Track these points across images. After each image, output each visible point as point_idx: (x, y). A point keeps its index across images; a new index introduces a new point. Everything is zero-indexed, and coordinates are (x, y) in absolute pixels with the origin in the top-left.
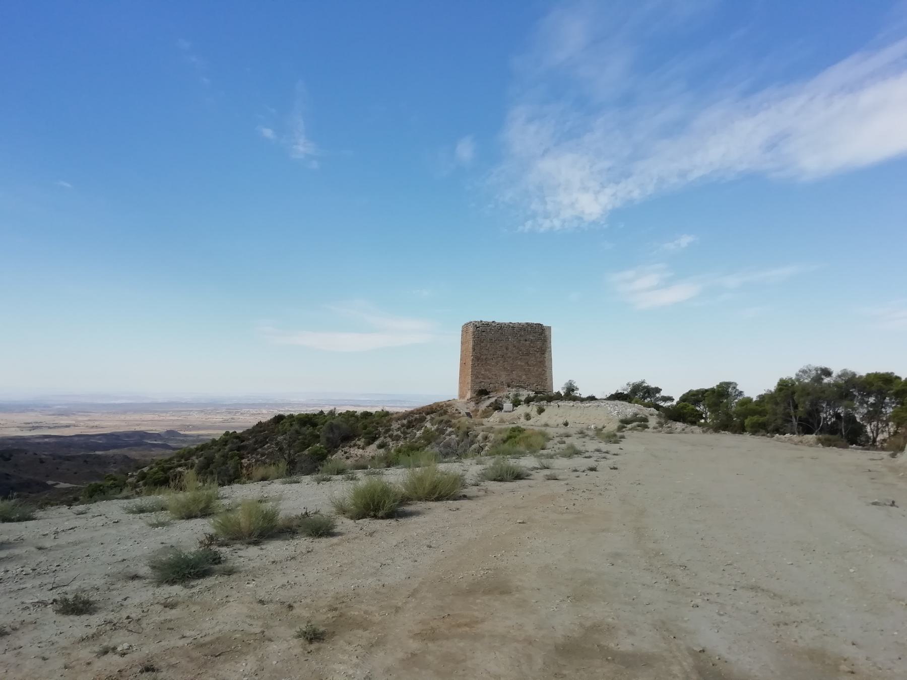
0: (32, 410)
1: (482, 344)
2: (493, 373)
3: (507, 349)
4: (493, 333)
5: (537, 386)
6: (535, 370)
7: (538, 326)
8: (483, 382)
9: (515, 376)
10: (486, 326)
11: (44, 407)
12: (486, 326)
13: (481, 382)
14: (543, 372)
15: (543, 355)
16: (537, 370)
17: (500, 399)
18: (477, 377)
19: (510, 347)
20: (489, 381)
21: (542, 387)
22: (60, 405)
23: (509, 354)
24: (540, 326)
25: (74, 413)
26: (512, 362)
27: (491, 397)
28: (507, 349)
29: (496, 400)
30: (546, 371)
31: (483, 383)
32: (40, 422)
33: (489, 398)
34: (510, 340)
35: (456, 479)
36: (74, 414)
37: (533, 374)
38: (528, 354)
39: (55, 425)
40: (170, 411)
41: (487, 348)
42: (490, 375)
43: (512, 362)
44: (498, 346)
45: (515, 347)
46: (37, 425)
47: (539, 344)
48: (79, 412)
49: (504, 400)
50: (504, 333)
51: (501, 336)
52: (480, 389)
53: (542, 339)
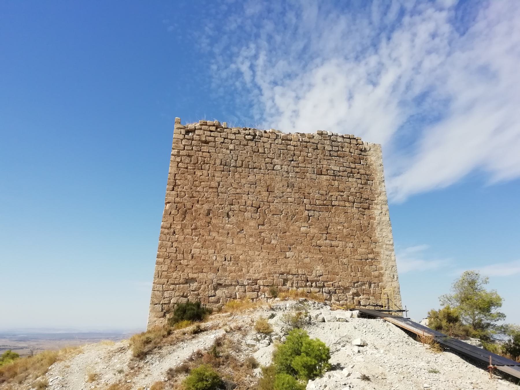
0: (4, 338)
1: (199, 173)
2: (228, 253)
3: (269, 190)
4: (231, 147)
5: (357, 294)
6: (348, 251)
7: (348, 140)
8: (193, 280)
9: (292, 267)
10: (213, 128)
11: (13, 335)
12: (213, 128)
13: (188, 281)
14: (371, 256)
15: (367, 212)
16: (354, 250)
17: (237, 336)
18: (177, 266)
19: (278, 186)
20: (211, 276)
21: (372, 300)
22: (23, 334)
23: (276, 205)
24: (354, 142)
25: (30, 339)
26: (281, 225)
27: (205, 330)
28: (269, 190)
29: (218, 343)
30: (378, 253)
31: (194, 285)
32: (6, 346)
33: (197, 332)
34: (278, 167)
35: (267, 368)
36: (29, 340)
37: (345, 261)
38: (327, 206)
39: (14, 348)
40: (88, 338)
41: (214, 184)
42: (218, 261)
43: (281, 225)
44: (243, 181)
45: (290, 185)
46: (3, 347)
47: (353, 183)
48: (32, 339)
49: (249, 340)
50: (261, 150)
51: (255, 159)
52: (184, 300)
53: (362, 171)
